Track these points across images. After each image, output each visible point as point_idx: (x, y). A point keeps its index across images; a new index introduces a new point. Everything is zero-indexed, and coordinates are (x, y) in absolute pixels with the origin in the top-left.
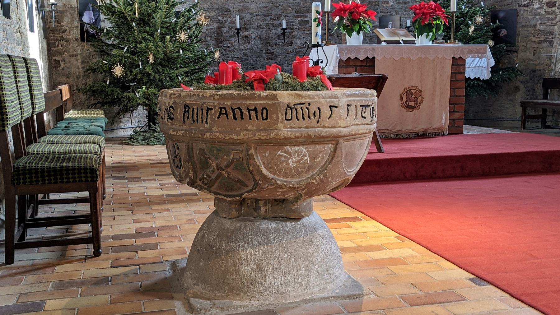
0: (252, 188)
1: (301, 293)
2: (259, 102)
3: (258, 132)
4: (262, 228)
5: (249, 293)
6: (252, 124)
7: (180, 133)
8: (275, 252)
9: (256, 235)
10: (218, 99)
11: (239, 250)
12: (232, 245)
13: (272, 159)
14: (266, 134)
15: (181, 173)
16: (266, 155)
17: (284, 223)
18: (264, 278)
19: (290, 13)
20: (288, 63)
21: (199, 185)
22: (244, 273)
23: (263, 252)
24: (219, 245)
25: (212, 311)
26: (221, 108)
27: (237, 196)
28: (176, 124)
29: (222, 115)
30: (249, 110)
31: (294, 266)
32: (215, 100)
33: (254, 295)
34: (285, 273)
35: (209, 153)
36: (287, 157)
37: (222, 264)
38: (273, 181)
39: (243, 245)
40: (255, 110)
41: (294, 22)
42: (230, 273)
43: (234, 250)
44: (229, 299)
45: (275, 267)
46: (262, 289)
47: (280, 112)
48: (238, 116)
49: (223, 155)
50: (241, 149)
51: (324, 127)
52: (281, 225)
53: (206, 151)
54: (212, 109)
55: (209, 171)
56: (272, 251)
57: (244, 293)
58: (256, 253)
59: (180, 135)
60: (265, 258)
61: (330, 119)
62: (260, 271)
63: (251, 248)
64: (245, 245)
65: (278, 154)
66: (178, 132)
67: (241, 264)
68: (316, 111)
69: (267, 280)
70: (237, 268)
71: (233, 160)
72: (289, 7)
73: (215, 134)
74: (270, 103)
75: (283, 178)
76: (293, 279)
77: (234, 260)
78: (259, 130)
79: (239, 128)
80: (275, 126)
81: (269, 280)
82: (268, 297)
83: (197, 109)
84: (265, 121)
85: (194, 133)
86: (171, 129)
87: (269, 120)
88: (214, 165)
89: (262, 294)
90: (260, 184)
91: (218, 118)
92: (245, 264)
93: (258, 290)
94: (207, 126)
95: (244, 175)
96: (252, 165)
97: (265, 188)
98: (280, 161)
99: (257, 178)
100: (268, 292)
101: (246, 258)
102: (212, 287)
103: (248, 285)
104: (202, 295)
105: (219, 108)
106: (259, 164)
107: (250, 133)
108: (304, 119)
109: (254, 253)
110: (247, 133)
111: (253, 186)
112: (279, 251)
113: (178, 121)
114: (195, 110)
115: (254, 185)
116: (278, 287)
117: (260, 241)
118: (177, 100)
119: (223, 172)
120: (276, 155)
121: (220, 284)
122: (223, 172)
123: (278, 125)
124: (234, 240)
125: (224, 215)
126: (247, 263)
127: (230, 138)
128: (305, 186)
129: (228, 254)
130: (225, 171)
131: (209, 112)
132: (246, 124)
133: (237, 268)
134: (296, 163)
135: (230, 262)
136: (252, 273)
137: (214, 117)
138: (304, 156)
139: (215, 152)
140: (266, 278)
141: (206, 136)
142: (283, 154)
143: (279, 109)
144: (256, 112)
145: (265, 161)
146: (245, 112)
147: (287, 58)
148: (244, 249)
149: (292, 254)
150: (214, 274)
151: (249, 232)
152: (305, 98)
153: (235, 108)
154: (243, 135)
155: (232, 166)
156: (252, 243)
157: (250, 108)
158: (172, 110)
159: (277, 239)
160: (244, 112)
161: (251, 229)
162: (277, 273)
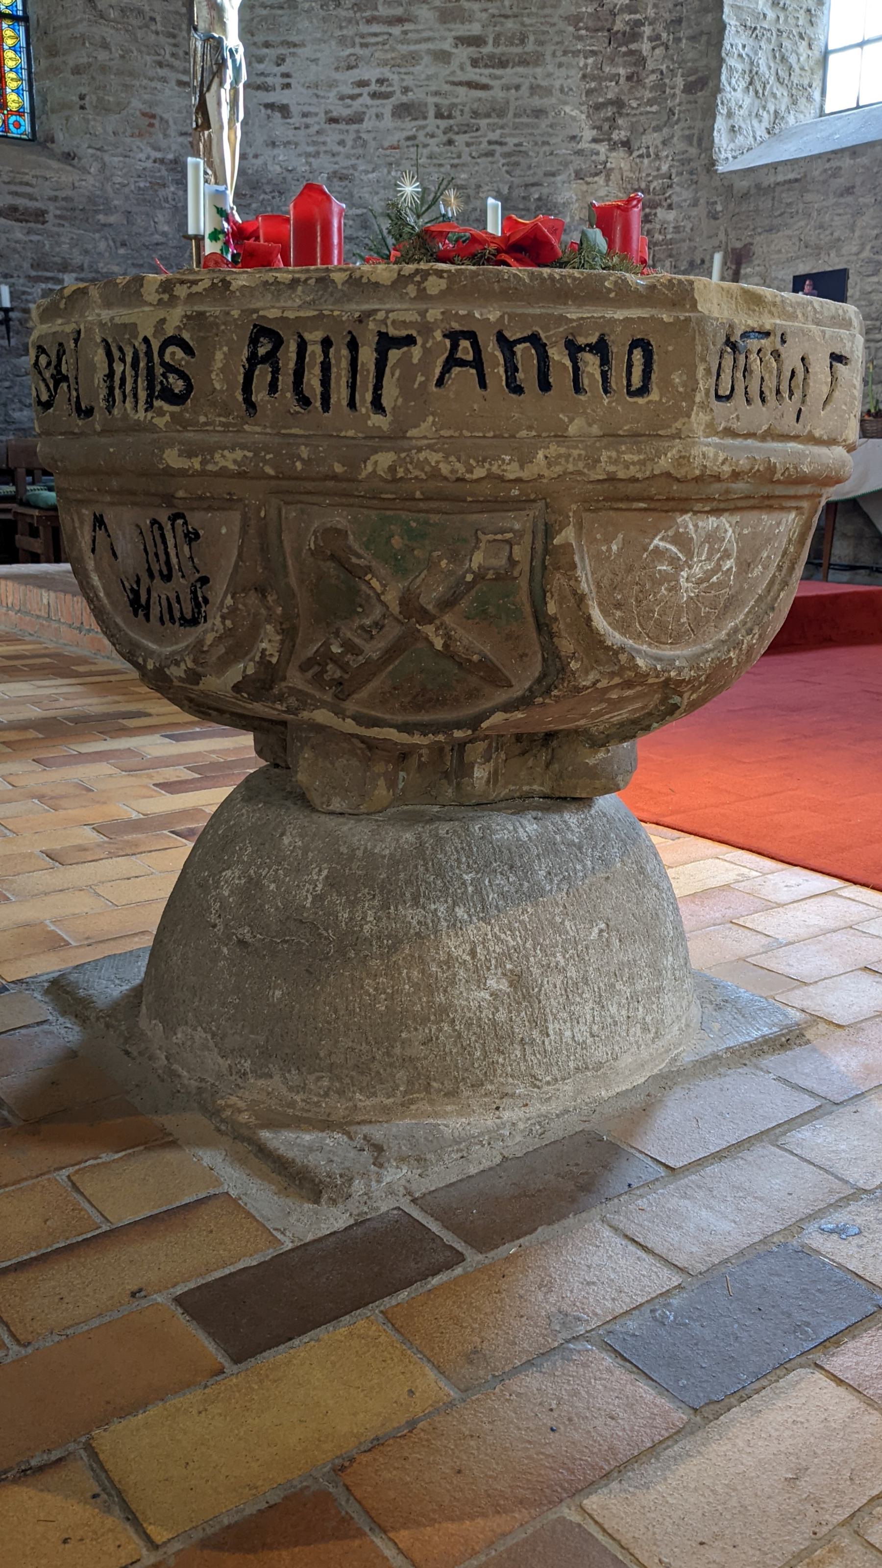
0: (530, 689)
1: (645, 1054)
2: (620, 314)
3: (606, 448)
4: (497, 840)
5: (492, 1082)
6: (585, 413)
7: (228, 460)
8: (562, 923)
9: (486, 868)
10: (443, 294)
11: (436, 932)
12: (405, 916)
13: (630, 569)
14: (642, 457)
15: (208, 642)
16: (609, 549)
17: (556, 818)
18: (538, 1022)
19: (19, 267)
20: (20, 401)
21: (293, 691)
22: (468, 1015)
23: (526, 929)
24: (351, 919)
25: (388, 1179)
26: (454, 337)
27: (458, 725)
28: (202, 419)
29: (456, 370)
30: (573, 349)
31: (621, 965)
32: (431, 298)
33: (508, 1089)
34: (600, 996)
35: (367, 548)
36: (679, 559)
37: (376, 989)
38: (623, 658)
39: (451, 910)
40: (601, 348)
41: (29, 294)
42: (415, 1020)
43: (418, 934)
44: (414, 1117)
45: (571, 978)
46: (535, 1061)
47: (703, 360)
48: (527, 375)
49: (435, 554)
50: (517, 526)
51: (812, 439)
52: (552, 823)
53: (351, 537)
54: (410, 341)
55: (356, 624)
56: (552, 924)
57: (472, 1086)
58: (503, 936)
59: (223, 473)
60: (535, 950)
61: (828, 408)
62: (524, 998)
63: (482, 919)
64: (457, 909)
65: (651, 547)
66: (217, 456)
67: (453, 982)
68: (797, 371)
69: (551, 1026)
70: (440, 998)
71: (480, 577)
72: (15, 250)
73: (422, 456)
74: (665, 317)
75: (650, 645)
76: (624, 1012)
77: (423, 972)
78: (612, 437)
79: (530, 428)
80: (678, 425)
81: (557, 1026)
82: (557, 1086)
83: (326, 343)
84: (641, 401)
85: (305, 456)
86: (172, 446)
87: (654, 396)
88: (391, 598)
89: (534, 1081)
90: (573, 673)
91: (440, 382)
92: (467, 981)
93: (523, 1068)
94: (376, 420)
95: (509, 637)
96: (556, 597)
97: (588, 688)
98: (652, 578)
99: (566, 645)
100: (555, 1070)
101: (468, 958)
102: (340, 1079)
103: (485, 1056)
104: (290, 1111)
105: (445, 336)
106: (586, 590)
107: (575, 452)
108: (763, 400)
109: (495, 936)
110: (563, 450)
111: (539, 681)
112: (574, 918)
113: (214, 404)
114: (314, 350)
115: (544, 675)
116: (583, 1045)
117: (506, 889)
118: (212, 309)
119: (429, 630)
120: (646, 550)
121: (375, 1066)
122: (429, 630)
123: (689, 416)
124: (408, 895)
125: (337, 804)
126: (475, 976)
127: (490, 476)
128: (707, 678)
129: (394, 948)
130: (438, 622)
131: (394, 355)
132: (562, 411)
133: (440, 998)
134: (699, 582)
135: (409, 978)
136: (498, 1011)
137: (420, 378)
138: (727, 555)
139: (397, 542)
140: (546, 1021)
141: (370, 468)
142: (669, 546)
143: (699, 348)
144: (605, 361)
145: (603, 577)
146: (558, 355)
147: (16, 389)
148: (455, 924)
149: (611, 924)
150: (342, 1028)
151: (458, 860)
152: (770, 312)
153: (519, 336)
154: (543, 463)
155: (463, 604)
156: (483, 901)
157: (581, 341)
158: (180, 354)
159: (556, 875)
160: (556, 358)
161: (462, 848)
162: (578, 999)
